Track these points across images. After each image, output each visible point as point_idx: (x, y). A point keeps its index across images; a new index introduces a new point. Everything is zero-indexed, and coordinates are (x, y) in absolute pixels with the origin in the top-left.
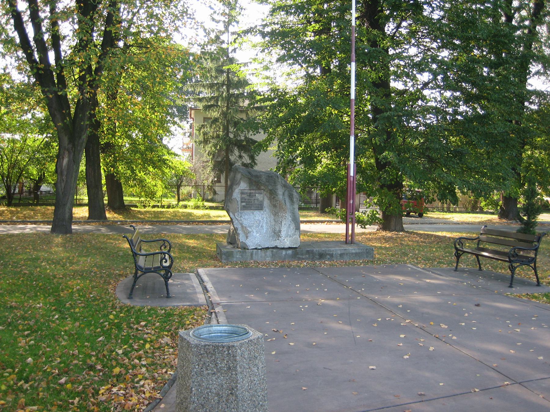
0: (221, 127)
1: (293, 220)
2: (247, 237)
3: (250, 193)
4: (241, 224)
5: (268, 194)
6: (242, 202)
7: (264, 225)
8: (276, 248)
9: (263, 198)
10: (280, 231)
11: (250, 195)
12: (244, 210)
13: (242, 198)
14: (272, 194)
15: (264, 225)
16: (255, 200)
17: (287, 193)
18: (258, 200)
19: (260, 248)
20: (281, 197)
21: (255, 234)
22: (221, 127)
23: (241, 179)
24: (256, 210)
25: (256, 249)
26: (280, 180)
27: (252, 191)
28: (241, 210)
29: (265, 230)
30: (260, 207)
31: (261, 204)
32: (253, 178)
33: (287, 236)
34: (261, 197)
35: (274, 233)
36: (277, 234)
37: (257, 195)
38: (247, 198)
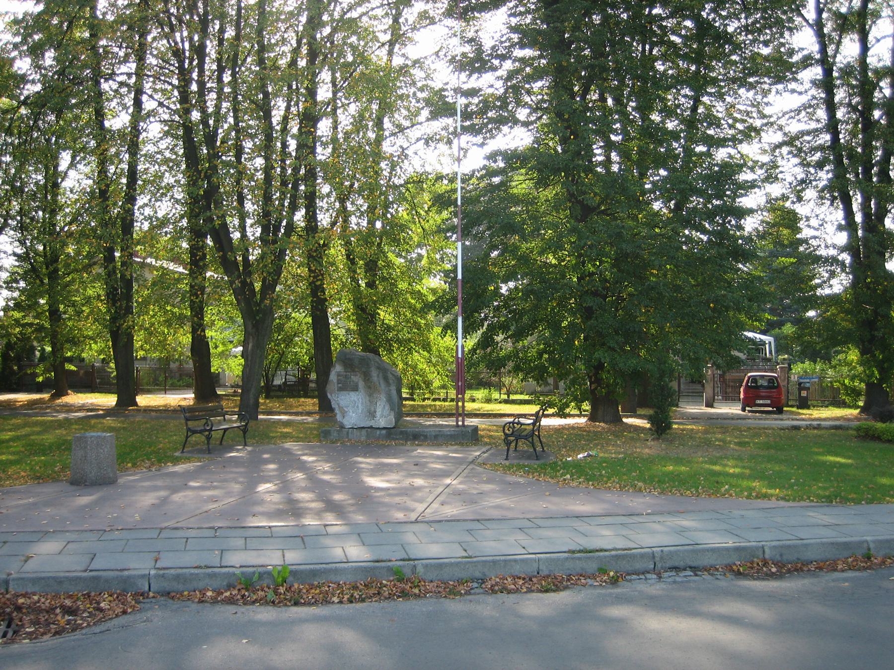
4: (338, 404)
8: (371, 427)
10: (375, 412)
13: (338, 380)
14: (367, 377)
17: (381, 375)
20: (375, 379)
30: (355, 389)
33: (382, 416)
36: (372, 414)
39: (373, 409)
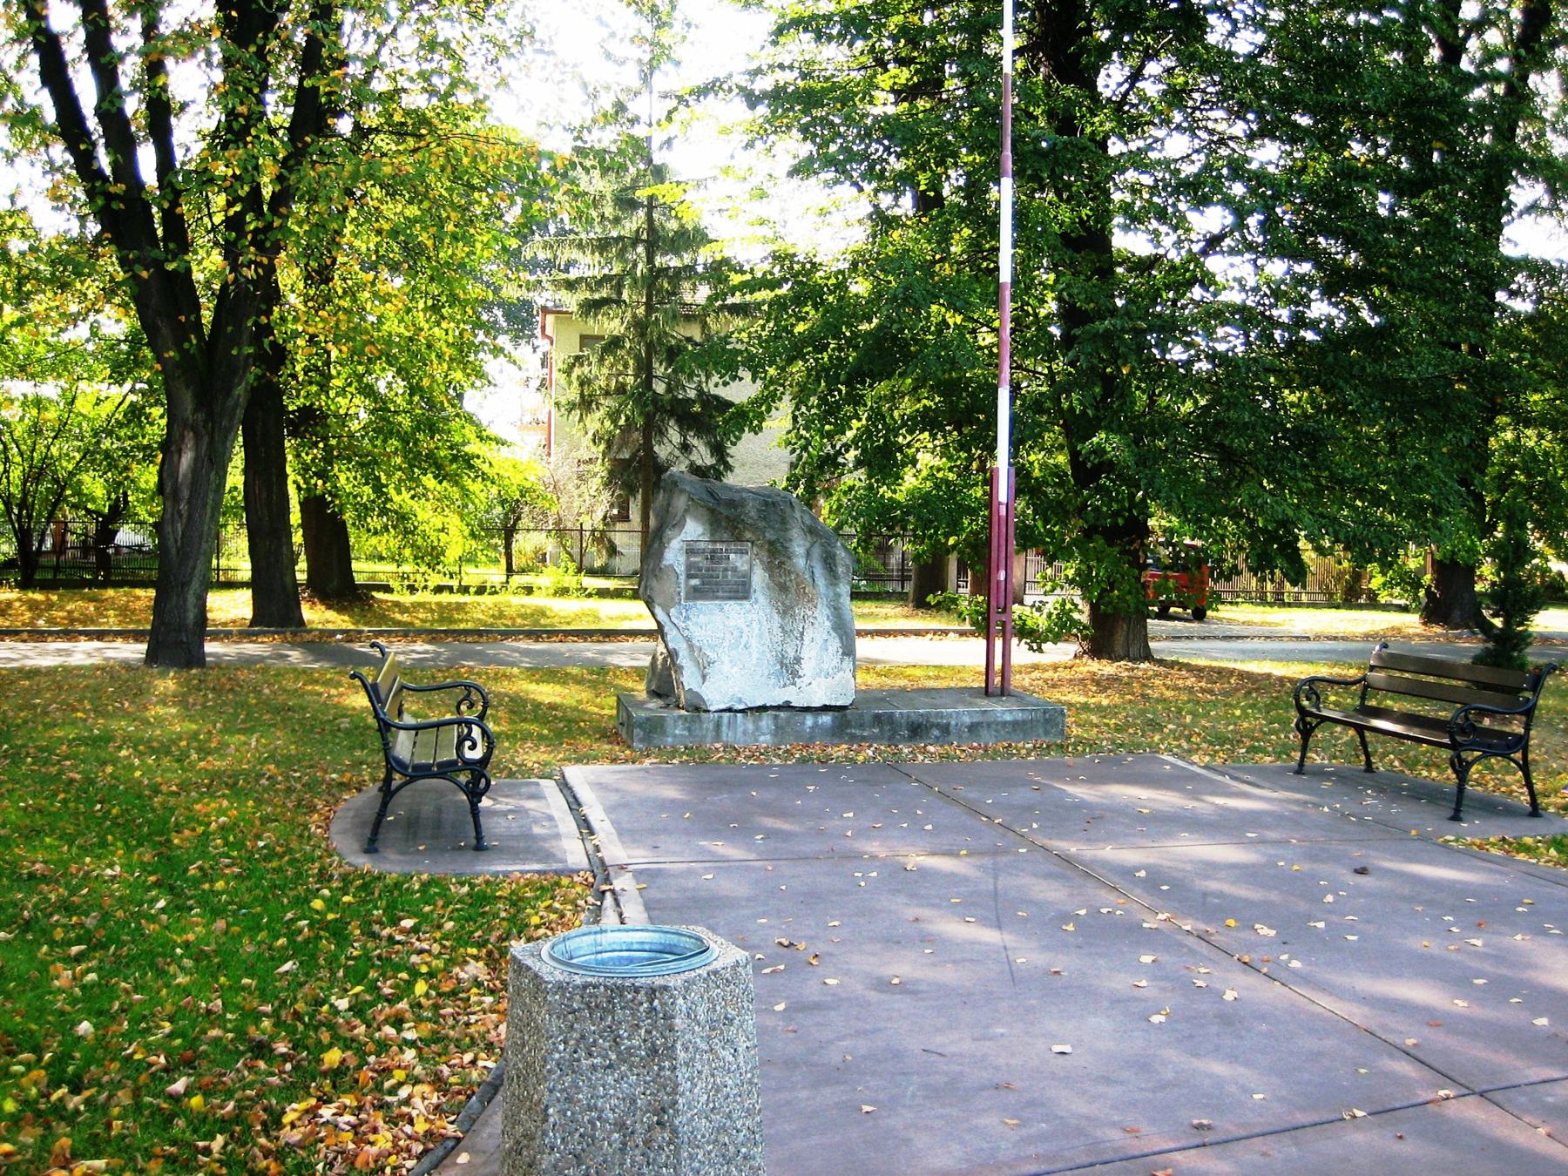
0: (631, 362)
1: (834, 629)
2: (704, 677)
3: (714, 551)
4: (688, 640)
5: (764, 555)
6: (689, 576)
7: (754, 643)
8: (787, 707)
9: (751, 566)
10: (798, 660)
11: (713, 556)
12: (696, 599)
13: (689, 566)
14: (776, 555)
15: (754, 643)
16: (726, 570)
17: (817, 551)
18: (735, 570)
19: (742, 707)
20: (801, 562)
21: (726, 668)
22: (631, 362)
23: (686, 511)
24: (730, 598)
25: (729, 710)
26: (798, 515)
27: (718, 546)
28: (687, 599)
29: (755, 655)
30: (741, 591)
31: (744, 584)
32: (721, 509)
34: (745, 561)
35: (782, 664)
36: (790, 668)
37: (732, 556)
38: (704, 564)
39: (791, 654)
